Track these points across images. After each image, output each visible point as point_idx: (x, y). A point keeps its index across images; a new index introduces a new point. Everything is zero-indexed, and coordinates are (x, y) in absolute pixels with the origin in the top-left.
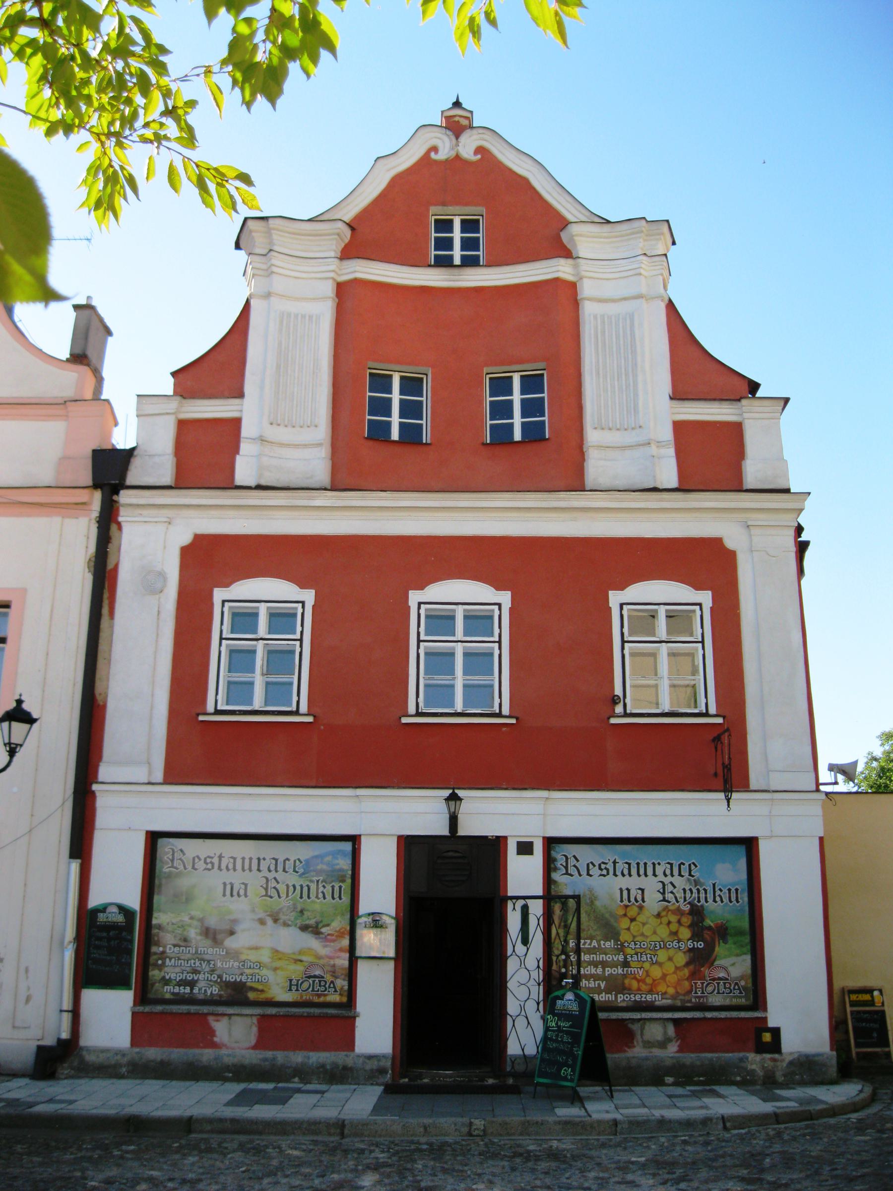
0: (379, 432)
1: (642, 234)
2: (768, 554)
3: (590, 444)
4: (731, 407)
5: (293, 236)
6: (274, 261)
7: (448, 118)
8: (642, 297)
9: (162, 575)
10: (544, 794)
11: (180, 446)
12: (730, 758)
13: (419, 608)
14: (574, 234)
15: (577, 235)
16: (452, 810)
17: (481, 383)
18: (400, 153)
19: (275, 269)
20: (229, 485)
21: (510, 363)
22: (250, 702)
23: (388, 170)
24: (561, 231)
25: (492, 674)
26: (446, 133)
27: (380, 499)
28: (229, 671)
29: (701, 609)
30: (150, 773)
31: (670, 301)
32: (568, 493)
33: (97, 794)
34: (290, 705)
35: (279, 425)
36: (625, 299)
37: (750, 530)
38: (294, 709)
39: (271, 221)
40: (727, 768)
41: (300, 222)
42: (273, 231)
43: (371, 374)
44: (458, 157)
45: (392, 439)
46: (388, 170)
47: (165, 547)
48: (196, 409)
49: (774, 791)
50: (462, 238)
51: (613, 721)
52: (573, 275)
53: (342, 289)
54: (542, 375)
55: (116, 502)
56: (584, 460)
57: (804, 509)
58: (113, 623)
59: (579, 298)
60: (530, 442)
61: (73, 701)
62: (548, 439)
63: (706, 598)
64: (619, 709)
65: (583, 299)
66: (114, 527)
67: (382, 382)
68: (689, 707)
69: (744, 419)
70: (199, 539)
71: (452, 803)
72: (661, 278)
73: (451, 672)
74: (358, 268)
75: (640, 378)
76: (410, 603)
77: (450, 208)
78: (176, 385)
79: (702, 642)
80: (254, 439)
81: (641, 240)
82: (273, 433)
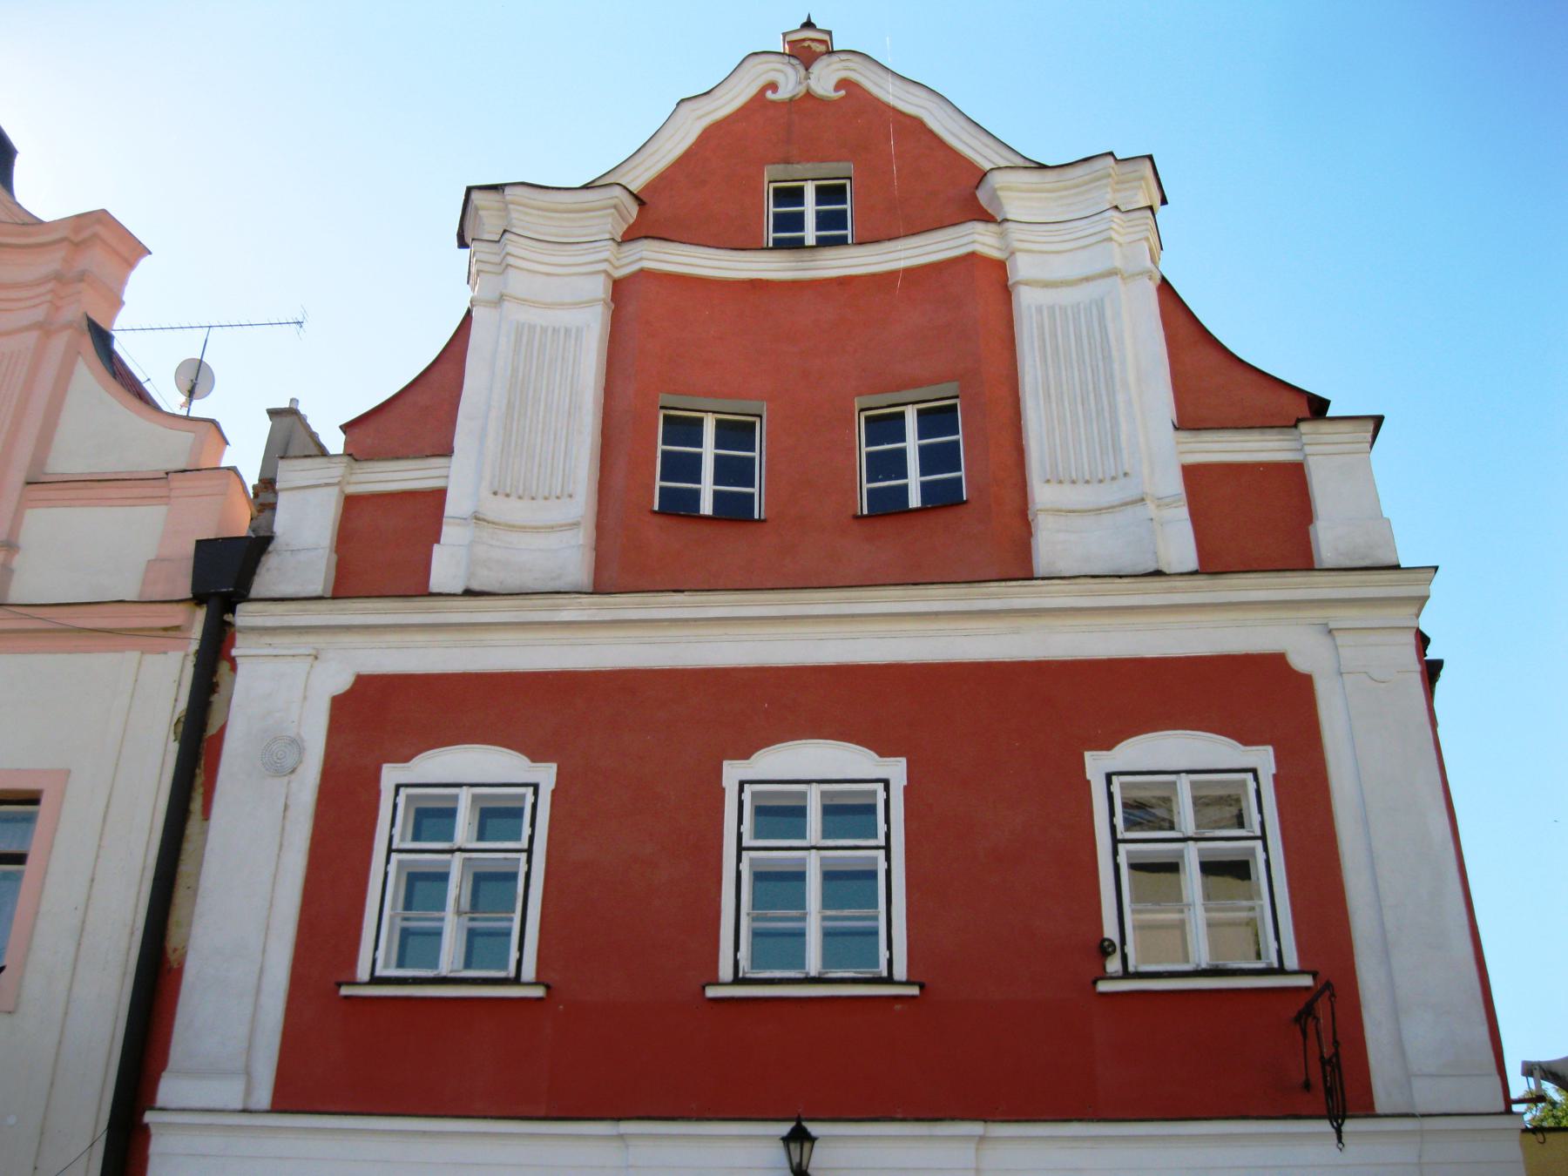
0: (680, 506)
1: (1110, 180)
2: (1373, 679)
3: (1039, 507)
4: (1281, 437)
5: (540, 213)
6: (510, 249)
7: (791, 43)
8: (1116, 274)
9: (297, 744)
10: (976, 1128)
11: (345, 537)
12: (1336, 1043)
13: (741, 790)
14: (997, 186)
15: (1002, 189)
16: (796, 1159)
17: (849, 422)
18: (717, 93)
19: (511, 260)
20: (417, 587)
21: (898, 389)
22: (434, 964)
23: (699, 118)
24: (977, 187)
25: (875, 905)
26: (789, 62)
27: (672, 606)
28: (408, 906)
29: (1256, 779)
30: (248, 1092)
31: (1164, 279)
32: (1003, 584)
33: (153, 1130)
34: (505, 967)
35: (508, 495)
36: (1087, 279)
37: (1334, 639)
38: (512, 972)
39: (508, 191)
40: (1332, 1064)
41: (554, 192)
42: (511, 206)
43: (666, 418)
44: (809, 95)
45: (701, 513)
46: (699, 118)
47: (305, 698)
49: (1423, 1116)
50: (818, 213)
51: (1103, 987)
52: (999, 249)
53: (620, 289)
54: (954, 407)
55: (230, 624)
56: (1030, 534)
57: (1428, 597)
58: (208, 826)
59: (1010, 283)
60: (933, 508)
61: (127, 961)
62: (966, 502)
63: (1263, 758)
64: (1113, 965)
65: (1017, 283)
66: (224, 667)
67: (684, 429)
68: (1246, 959)
69: (1306, 455)
70: (364, 684)
71: (795, 1147)
72: (1145, 245)
73: (800, 902)
74: (645, 254)
75: (1120, 398)
76: (725, 783)
77: (799, 166)
78: (346, 444)
79: (1263, 838)
80: (465, 519)
81: (1109, 189)
82: (496, 508)
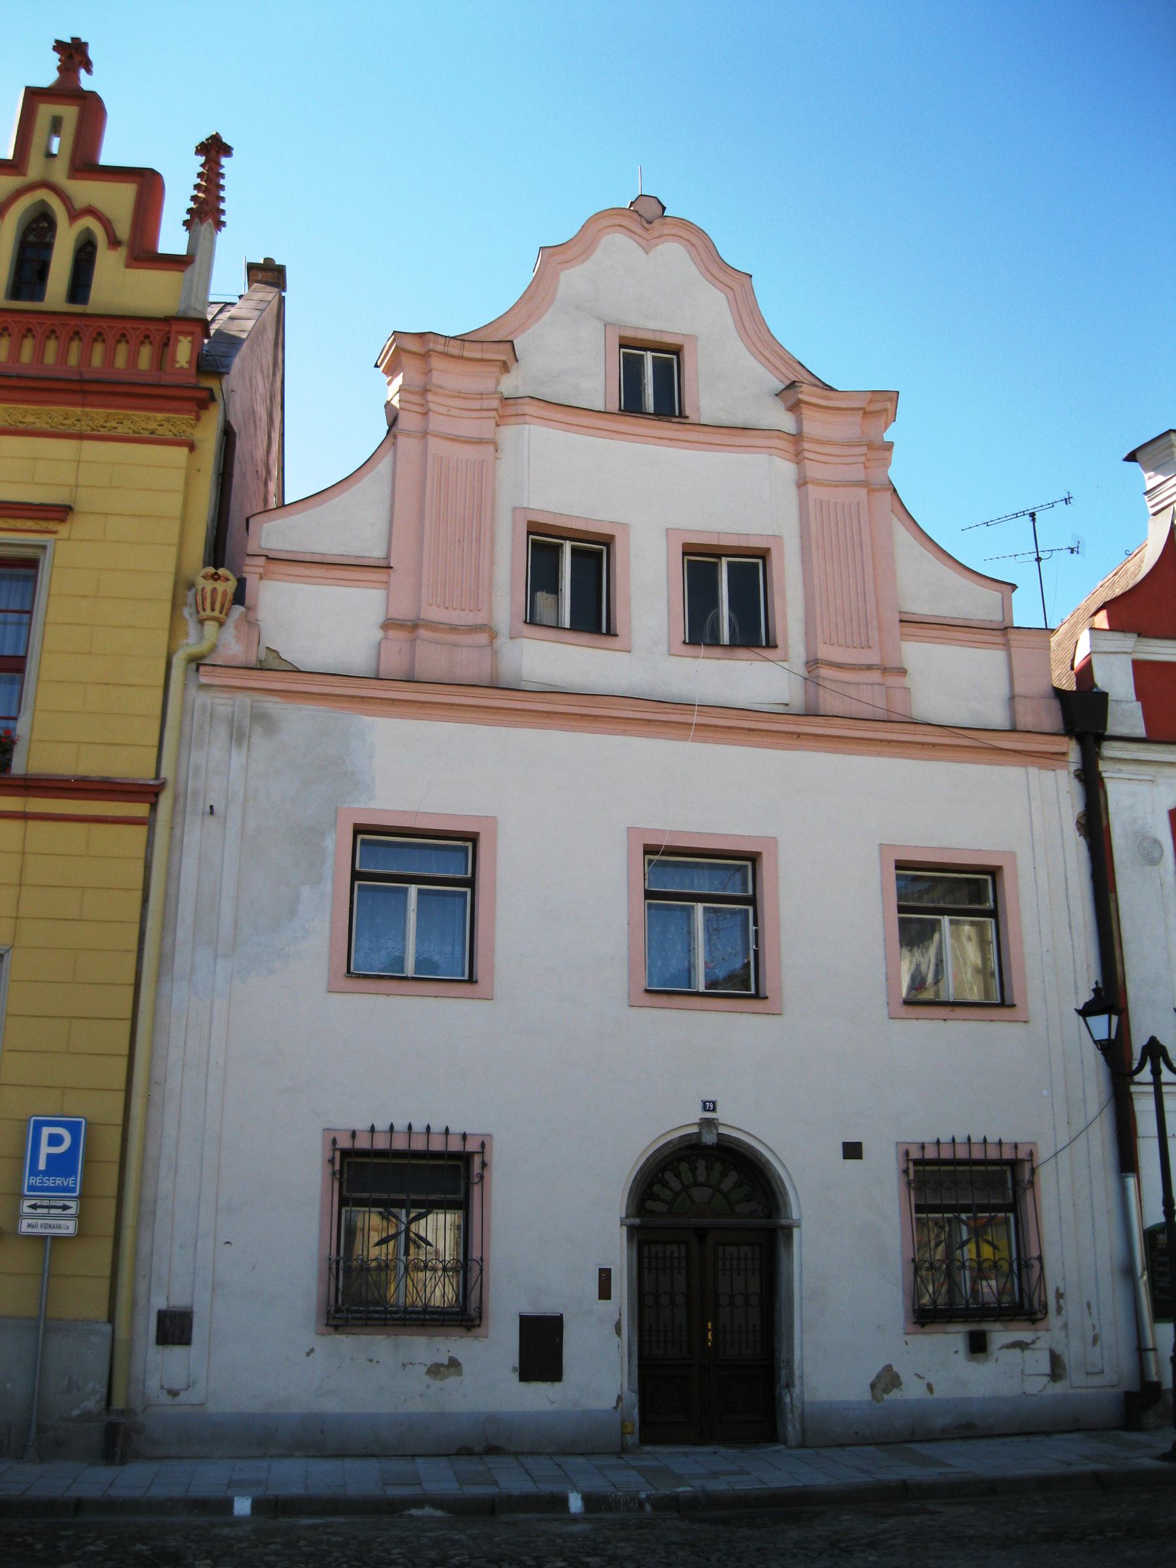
48: (1151, 649)
